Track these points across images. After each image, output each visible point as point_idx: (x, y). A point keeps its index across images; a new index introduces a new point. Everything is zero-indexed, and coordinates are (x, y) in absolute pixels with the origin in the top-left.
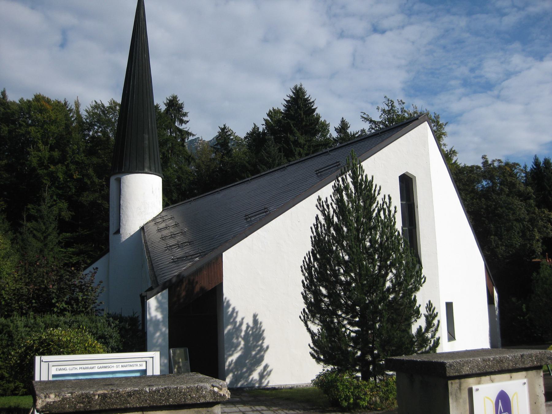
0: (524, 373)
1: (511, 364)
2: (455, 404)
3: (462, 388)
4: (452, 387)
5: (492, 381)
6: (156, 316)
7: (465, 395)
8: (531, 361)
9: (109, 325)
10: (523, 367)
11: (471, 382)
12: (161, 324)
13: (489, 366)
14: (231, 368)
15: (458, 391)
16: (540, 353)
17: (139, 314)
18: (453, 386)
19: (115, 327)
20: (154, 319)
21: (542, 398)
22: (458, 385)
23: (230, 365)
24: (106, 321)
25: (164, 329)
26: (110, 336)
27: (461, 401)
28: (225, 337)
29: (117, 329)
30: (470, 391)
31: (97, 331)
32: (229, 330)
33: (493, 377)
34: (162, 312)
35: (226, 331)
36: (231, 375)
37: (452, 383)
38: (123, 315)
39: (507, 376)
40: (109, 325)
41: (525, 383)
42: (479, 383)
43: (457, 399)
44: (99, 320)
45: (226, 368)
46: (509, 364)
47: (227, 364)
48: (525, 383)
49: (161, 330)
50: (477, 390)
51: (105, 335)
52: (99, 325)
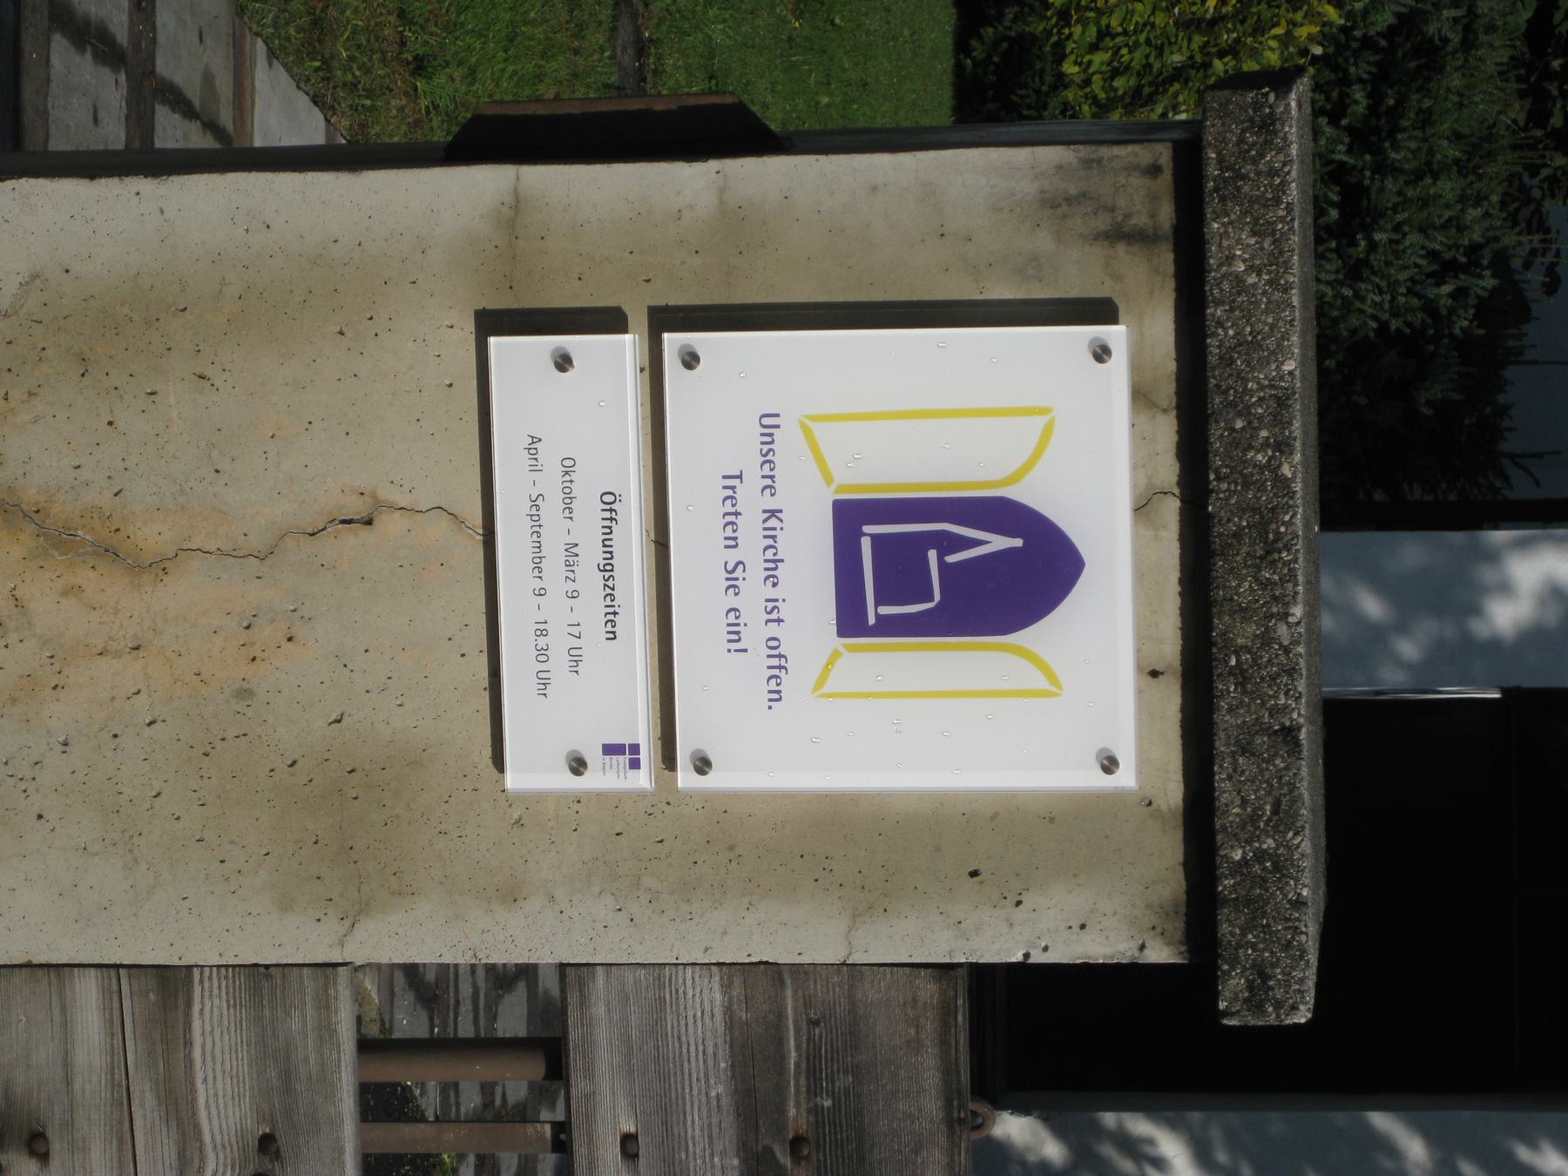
0: (1173, 793)
1: (1246, 633)
2: (1028, 188)
3: (1121, 248)
4: (1132, 168)
5: (1142, 508)
6: (1505, 588)
7: (1078, 277)
8: (1254, 819)
9: (1445, 268)
10: (1221, 746)
11: (1142, 335)
12: (1449, 632)
13: (1240, 442)
14: (1108, 1151)
15: (1103, 222)
16: (1299, 903)
17: (1521, 488)
18: (1138, 182)
19: (1430, 308)
20: (1487, 574)
21: (1002, 941)
22: (1141, 220)
23: (1134, 1148)
24: (1474, 249)
25: (1408, 649)
26: (1365, 262)
27: (1043, 241)
28: (1340, 1118)
29: (1418, 318)
30: (1099, 311)
31: (1395, 170)
32: (1394, 1152)
33: (1171, 509)
34: (1532, 637)
35: (1382, 1121)
36: (1053, 1150)
37: (1154, 170)
38: (1510, 373)
39: (1170, 647)
40: (1445, 268)
41: (1109, 765)
42: (1141, 396)
43: (1056, 205)
44: (1479, 200)
45: (1109, 1119)
46: (1245, 613)
47: (1140, 1126)
48: (1109, 765)
49: (1402, 628)
50: (1101, 353)
51: (1368, 230)
52: (1447, 187)
